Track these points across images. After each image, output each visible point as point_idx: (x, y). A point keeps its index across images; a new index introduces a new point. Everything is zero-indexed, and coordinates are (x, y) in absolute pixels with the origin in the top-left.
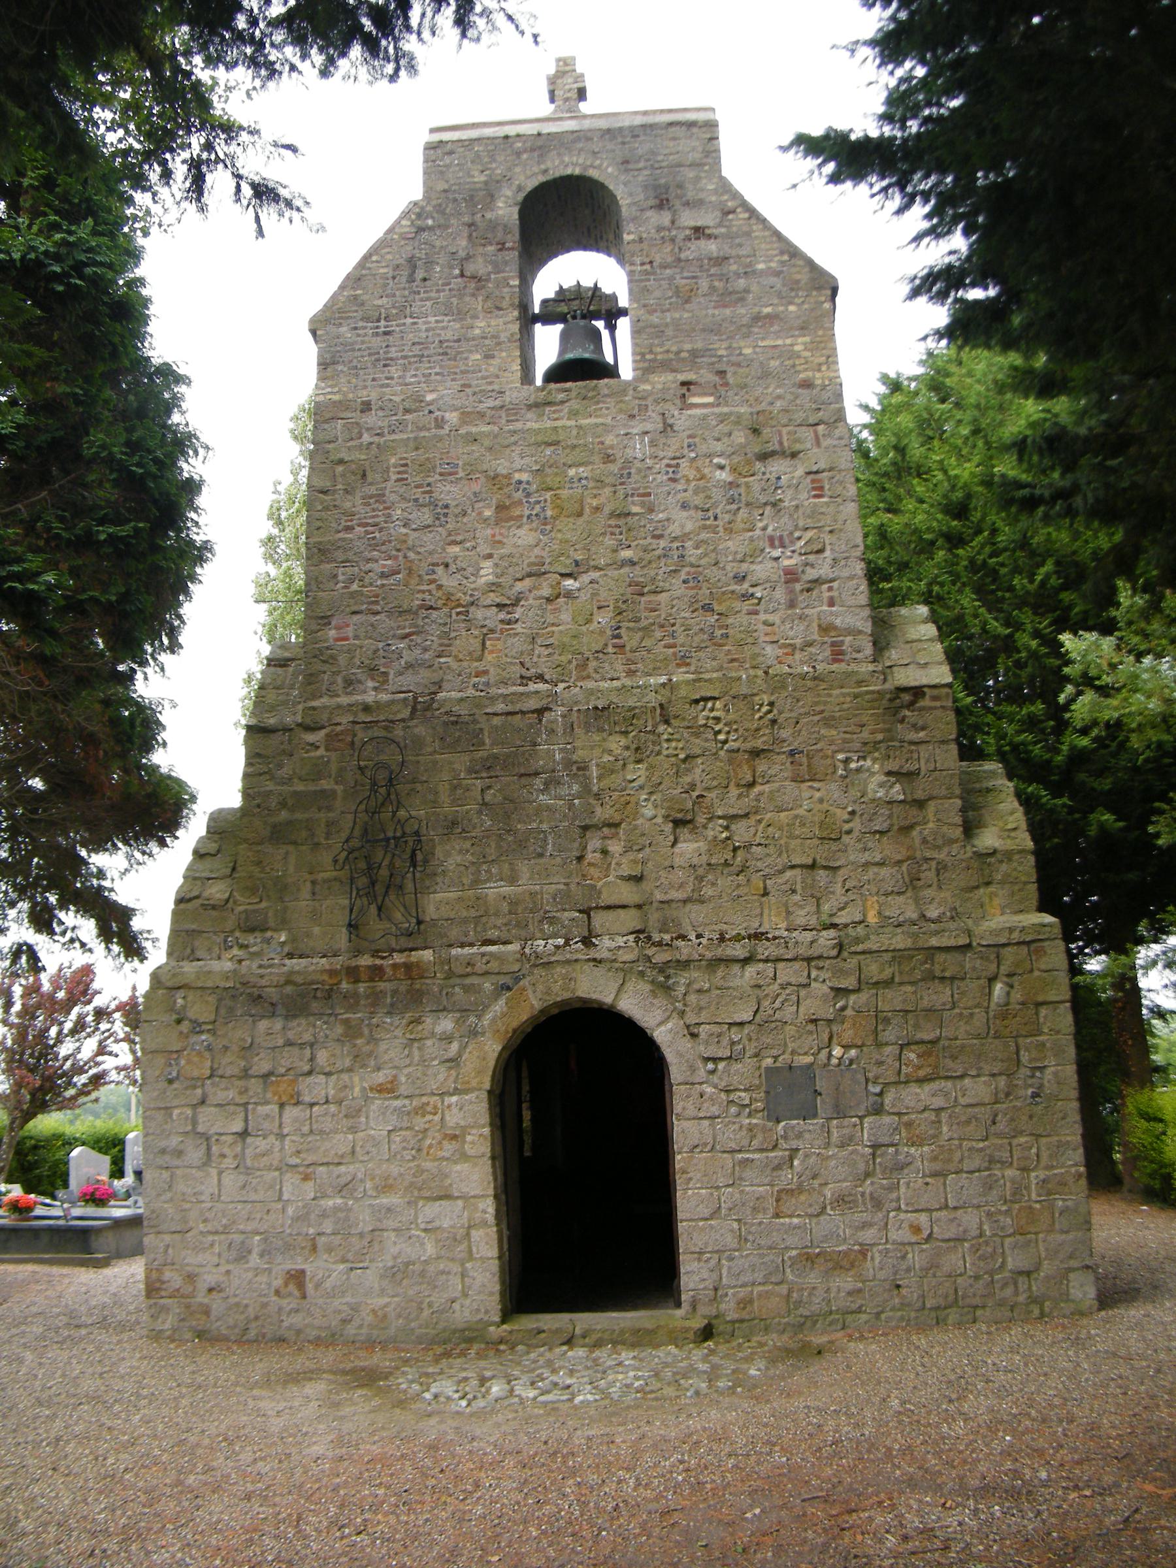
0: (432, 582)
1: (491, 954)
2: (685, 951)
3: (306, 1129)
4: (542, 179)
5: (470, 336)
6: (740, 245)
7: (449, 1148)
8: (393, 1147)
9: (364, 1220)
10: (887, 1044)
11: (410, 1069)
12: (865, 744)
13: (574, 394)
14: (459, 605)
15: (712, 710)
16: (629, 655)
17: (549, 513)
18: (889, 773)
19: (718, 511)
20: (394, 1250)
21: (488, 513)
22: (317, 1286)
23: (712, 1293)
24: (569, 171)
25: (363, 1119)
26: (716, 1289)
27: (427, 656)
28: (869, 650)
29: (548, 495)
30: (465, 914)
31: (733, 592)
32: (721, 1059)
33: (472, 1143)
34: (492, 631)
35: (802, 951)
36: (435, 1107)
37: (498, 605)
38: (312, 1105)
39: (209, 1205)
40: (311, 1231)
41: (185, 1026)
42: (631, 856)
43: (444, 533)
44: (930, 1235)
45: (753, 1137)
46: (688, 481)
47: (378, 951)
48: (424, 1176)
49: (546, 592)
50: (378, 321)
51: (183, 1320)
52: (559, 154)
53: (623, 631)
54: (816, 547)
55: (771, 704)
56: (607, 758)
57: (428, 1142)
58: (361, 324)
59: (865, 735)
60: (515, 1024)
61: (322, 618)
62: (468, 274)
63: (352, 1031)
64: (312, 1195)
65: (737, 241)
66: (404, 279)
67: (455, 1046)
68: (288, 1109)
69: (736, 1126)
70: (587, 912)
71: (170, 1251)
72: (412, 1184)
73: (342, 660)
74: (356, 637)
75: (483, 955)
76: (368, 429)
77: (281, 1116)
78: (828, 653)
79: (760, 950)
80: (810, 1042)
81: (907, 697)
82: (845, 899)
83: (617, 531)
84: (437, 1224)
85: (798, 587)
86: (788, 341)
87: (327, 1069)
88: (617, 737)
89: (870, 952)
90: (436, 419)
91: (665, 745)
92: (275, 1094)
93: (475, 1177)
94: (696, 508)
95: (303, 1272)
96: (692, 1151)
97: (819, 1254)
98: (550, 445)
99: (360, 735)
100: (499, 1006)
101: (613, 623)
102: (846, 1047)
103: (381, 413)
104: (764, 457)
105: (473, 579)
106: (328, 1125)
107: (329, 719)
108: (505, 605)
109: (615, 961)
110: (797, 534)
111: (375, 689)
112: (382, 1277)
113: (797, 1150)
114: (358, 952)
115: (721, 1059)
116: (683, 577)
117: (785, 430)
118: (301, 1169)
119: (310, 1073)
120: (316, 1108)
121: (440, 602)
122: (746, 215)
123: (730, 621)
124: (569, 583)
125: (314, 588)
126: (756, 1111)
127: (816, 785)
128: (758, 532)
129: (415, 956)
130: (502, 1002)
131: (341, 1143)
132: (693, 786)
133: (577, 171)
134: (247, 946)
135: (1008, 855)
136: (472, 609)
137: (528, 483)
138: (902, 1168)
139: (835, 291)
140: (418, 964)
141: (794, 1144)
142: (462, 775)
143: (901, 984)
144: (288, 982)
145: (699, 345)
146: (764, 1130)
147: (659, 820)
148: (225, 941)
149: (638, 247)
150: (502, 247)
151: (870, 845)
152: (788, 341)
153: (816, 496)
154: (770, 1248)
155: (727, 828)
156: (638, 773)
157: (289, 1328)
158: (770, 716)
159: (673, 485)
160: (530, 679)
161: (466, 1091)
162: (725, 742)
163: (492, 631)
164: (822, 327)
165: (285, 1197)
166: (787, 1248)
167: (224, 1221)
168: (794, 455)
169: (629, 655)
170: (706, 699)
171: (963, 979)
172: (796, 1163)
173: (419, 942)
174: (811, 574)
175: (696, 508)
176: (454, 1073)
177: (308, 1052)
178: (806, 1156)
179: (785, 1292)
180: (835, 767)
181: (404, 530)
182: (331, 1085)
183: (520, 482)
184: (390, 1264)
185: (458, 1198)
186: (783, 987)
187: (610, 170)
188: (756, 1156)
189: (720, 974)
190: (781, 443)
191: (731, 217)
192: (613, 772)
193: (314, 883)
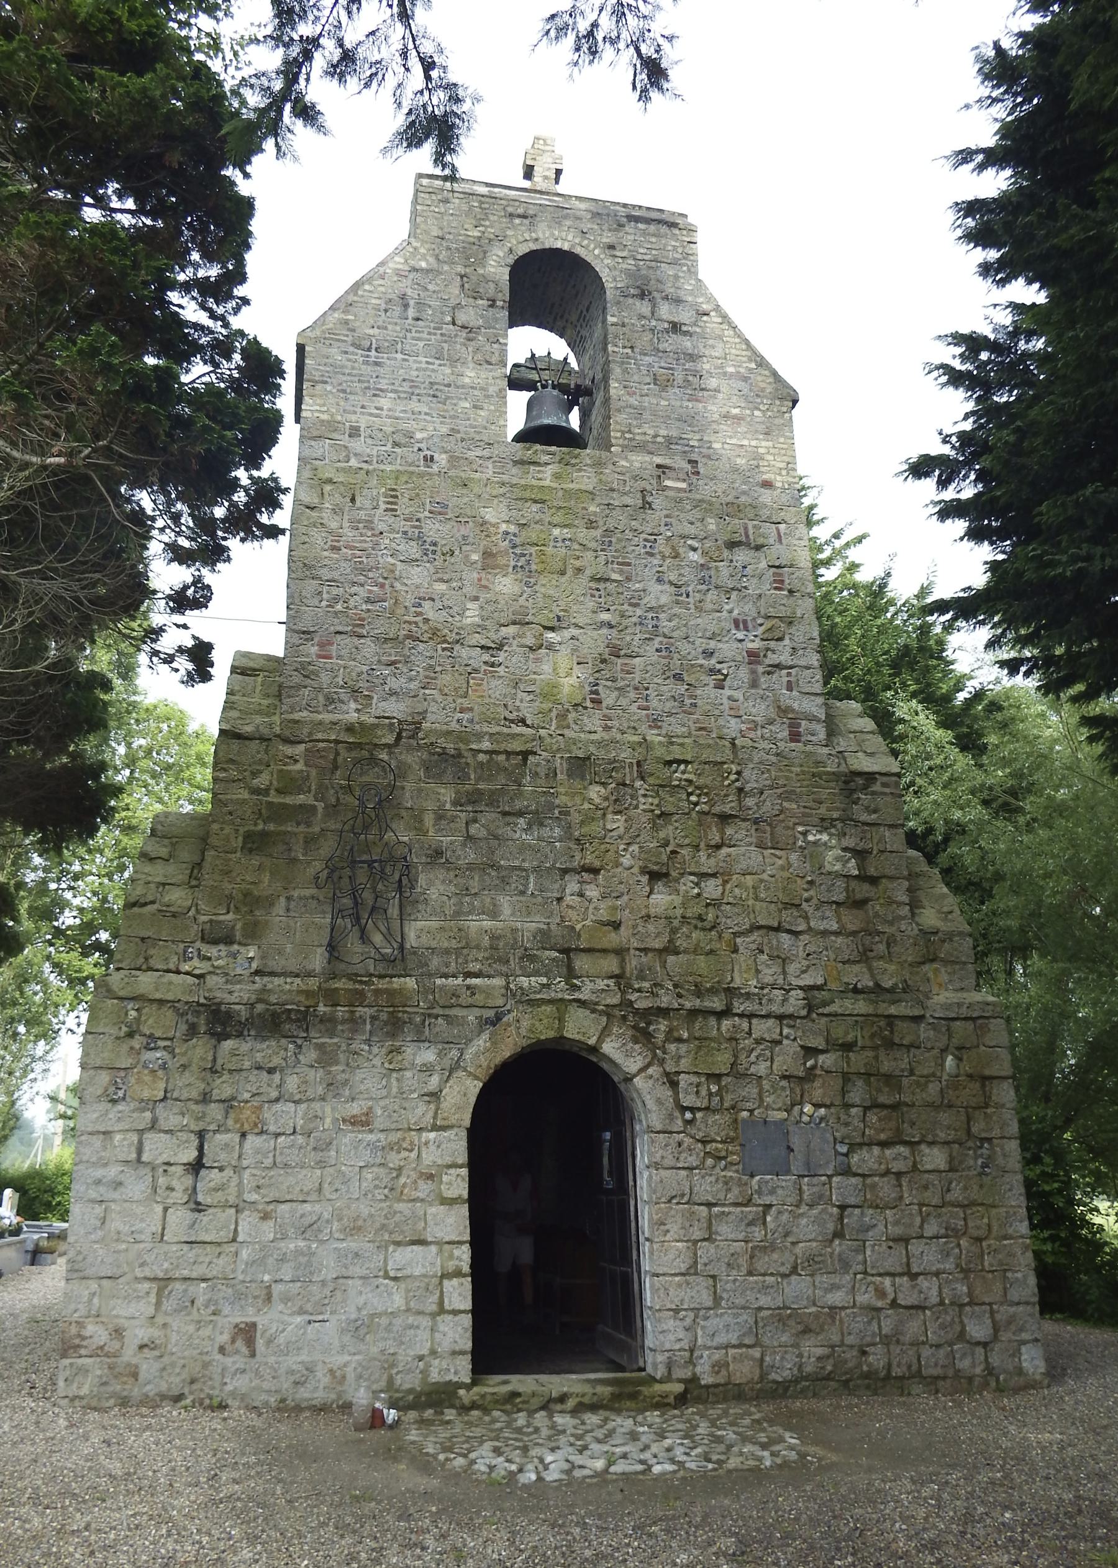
0: (418, 614)
1: (475, 987)
2: (664, 999)
3: (268, 1162)
4: (534, 247)
5: (459, 383)
6: (713, 347)
7: (425, 1188)
8: (364, 1184)
9: (328, 1267)
10: (853, 1106)
11: (387, 1101)
12: (823, 820)
13: (558, 458)
14: (445, 641)
15: (683, 772)
16: (606, 711)
17: (534, 567)
18: (845, 849)
19: (690, 589)
20: (361, 1300)
21: (475, 557)
22: (269, 1342)
23: (687, 1354)
24: (558, 245)
25: (333, 1153)
26: (692, 1351)
27: (413, 685)
28: (822, 735)
29: (533, 550)
30: (446, 944)
31: (701, 666)
32: (699, 1109)
33: (450, 1184)
34: (476, 671)
35: (775, 1008)
36: (412, 1143)
37: (482, 647)
38: (277, 1135)
39: (149, 1246)
40: (266, 1278)
41: (137, 1042)
42: (609, 902)
43: (432, 570)
44: (894, 1301)
45: (729, 1190)
46: (664, 558)
47: (357, 975)
48: (397, 1218)
49: (530, 641)
50: (369, 350)
51: (105, 1384)
52: (550, 227)
53: (600, 688)
54: (778, 635)
55: (739, 773)
56: (586, 806)
57: (402, 1180)
58: (351, 349)
59: (823, 811)
60: (498, 1060)
61: (304, 632)
62: (459, 322)
63: (326, 1058)
64: (271, 1236)
65: (711, 342)
66: (397, 314)
67: (434, 1081)
68: (250, 1138)
69: (713, 1179)
70: (566, 951)
71: (96, 1300)
72: (383, 1226)
73: (325, 678)
74: (339, 657)
75: (468, 987)
76: (356, 455)
77: (241, 1144)
78: (786, 733)
79: (736, 1004)
80: (785, 1098)
81: (860, 781)
82: (806, 963)
83: (597, 593)
84: (408, 1272)
85: (760, 669)
86: (754, 443)
87: (297, 1098)
88: (598, 788)
89: (836, 1015)
90: (425, 457)
91: (642, 800)
92: (236, 1122)
93: (451, 1220)
94: (671, 583)
95: (254, 1325)
96: (669, 1201)
97: (790, 1316)
98: (535, 502)
99: (343, 753)
100: (482, 1042)
101: (591, 680)
102: (817, 1106)
103: (369, 441)
104: (732, 545)
105: (458, 618)
106: (293, 1158)
107: (310, 734)
108: (489, 648)
109: (597, 1004)
110: (760, 621)
111: (358, 711)
112: (343, 1331)
113: (770, 1206)
114: (334, 976)
115: (699, 1109)
116: (657, 646)
117: (750, 524)
118: (260, 1207)
119: (277, 1100)
120: (281, 1139)
121: (426, 635)
122: (719, 320)
123: (699, 692)
124: (550, 635)
125: (297, 601)
126: (732, 1164)
127: (778, 852)
128: (725, 613)
129: (397, 983)
130: (485, 1036)
131: (309, 1178)
132: (666, 844)
133: (566, 247)
134: (209, 959)
135: (950, 936)
136: (457, 647)
137: (515, 535)
138: (867, 1231)
139: (795, 402)
140: (400, 991)
141: (767, 1200)
142: (448, 806)
143: (863, 1048)
144: (259, 1001)
145: (674, 433)
146: (741, 1184)
147: (636, 870)
148: (185, 952)
149: (621, 330)
150: (493, 303)
151: (828, 913)
152: (754, 443)
153: (776, 588)
154: (744, 1308)
155: (697, 884)
156: (616, 823)
157: (233, 1394)
158: (737, 784)
159: (650, 559)
160: (512, 721)
161: (443, 1128)
162: (696, 804)
163: (476, 671)
164: (783, 436)
165: (240, 1239)
166: (760, 1309)
167: (166, 1265)
168: (758, 548)
169: (606, 711)
170: (679, 762)
171: (919, 1047)
172: (769, 1219)
173: (399, 969)
174: (772, 658)
175: (671, 583)
176: (432, 1106)
177: (277, 1077)
178: (779, 1212)
179: (758, 1355)
180: (796, 839)
181: (390, 560)
182: (300, 1114)
183: (507, 533)
184: (353, 1316)
185: (431, 1243)
186: (758, 1042)
187: (597, 252)
188: (732, 1209)
189: (697, 1025)
190: (747, 536)
191: (705, 318)
192: (593, 819)
193: (288, 899)
